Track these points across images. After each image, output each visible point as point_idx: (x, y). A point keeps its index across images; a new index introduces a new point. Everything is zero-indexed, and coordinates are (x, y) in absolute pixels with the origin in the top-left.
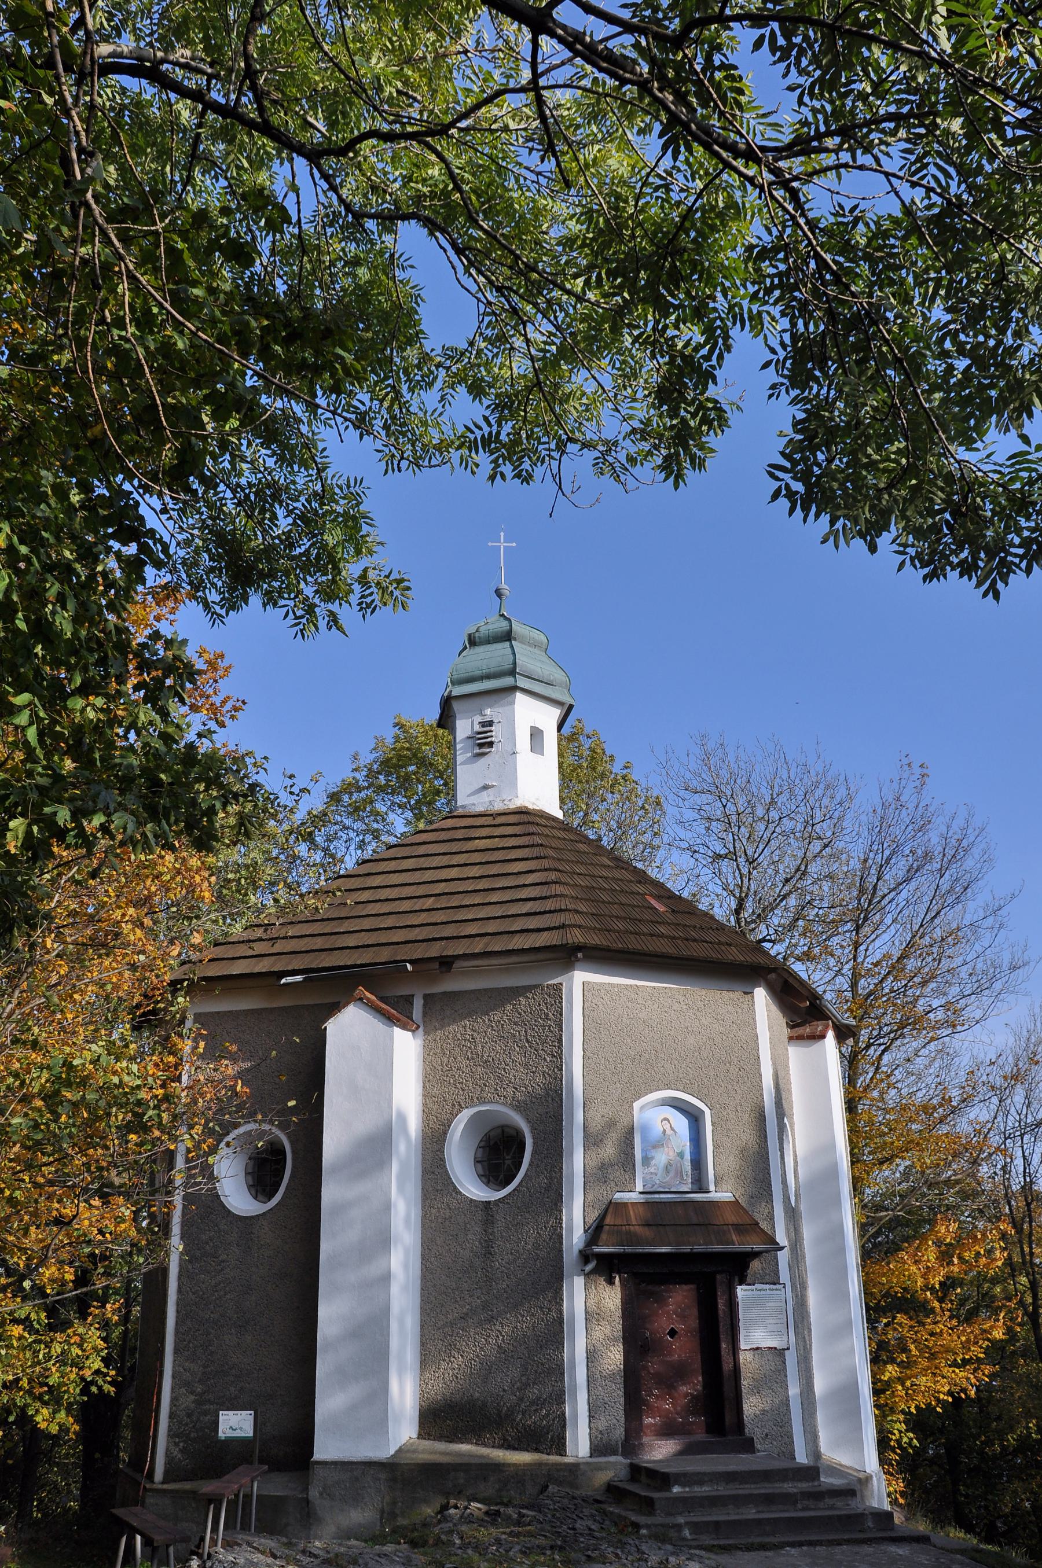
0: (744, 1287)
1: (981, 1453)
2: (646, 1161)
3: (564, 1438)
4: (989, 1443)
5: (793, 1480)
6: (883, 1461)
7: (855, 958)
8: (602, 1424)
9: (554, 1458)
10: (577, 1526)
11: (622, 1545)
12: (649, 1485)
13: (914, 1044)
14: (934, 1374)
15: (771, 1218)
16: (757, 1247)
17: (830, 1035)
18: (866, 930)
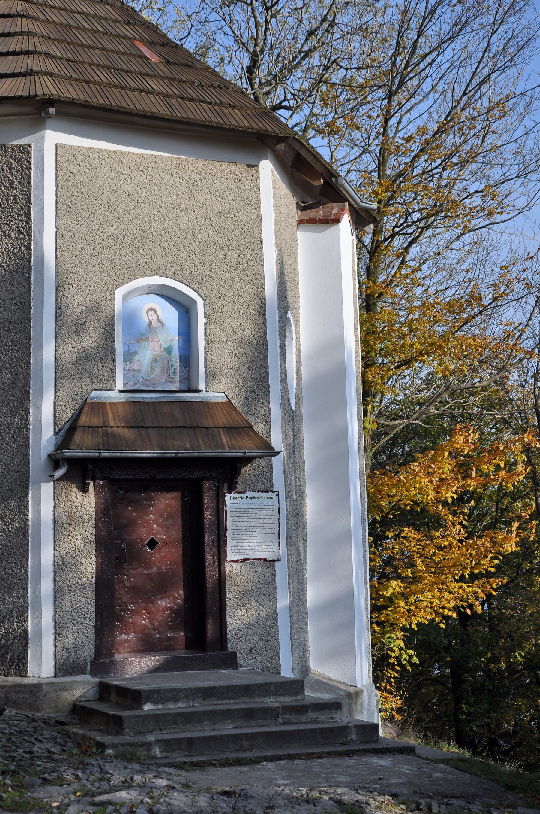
0: (234, 495)
1: (488, 672)
2: (129, 356)
3: (25, 658)
4: (495, 660)
5: (276, 694)
6: (377, 680)
7: (384, 133)
8: (69, 640)
9: (14, 680)
10: (35, 749)
11: (84, 766)
12: (118, 704)
13: (447, 236)
14: (440, 590)
15: (267, 419)
16: (249, 452)
17: (346, 219)
18: (401, 97)
